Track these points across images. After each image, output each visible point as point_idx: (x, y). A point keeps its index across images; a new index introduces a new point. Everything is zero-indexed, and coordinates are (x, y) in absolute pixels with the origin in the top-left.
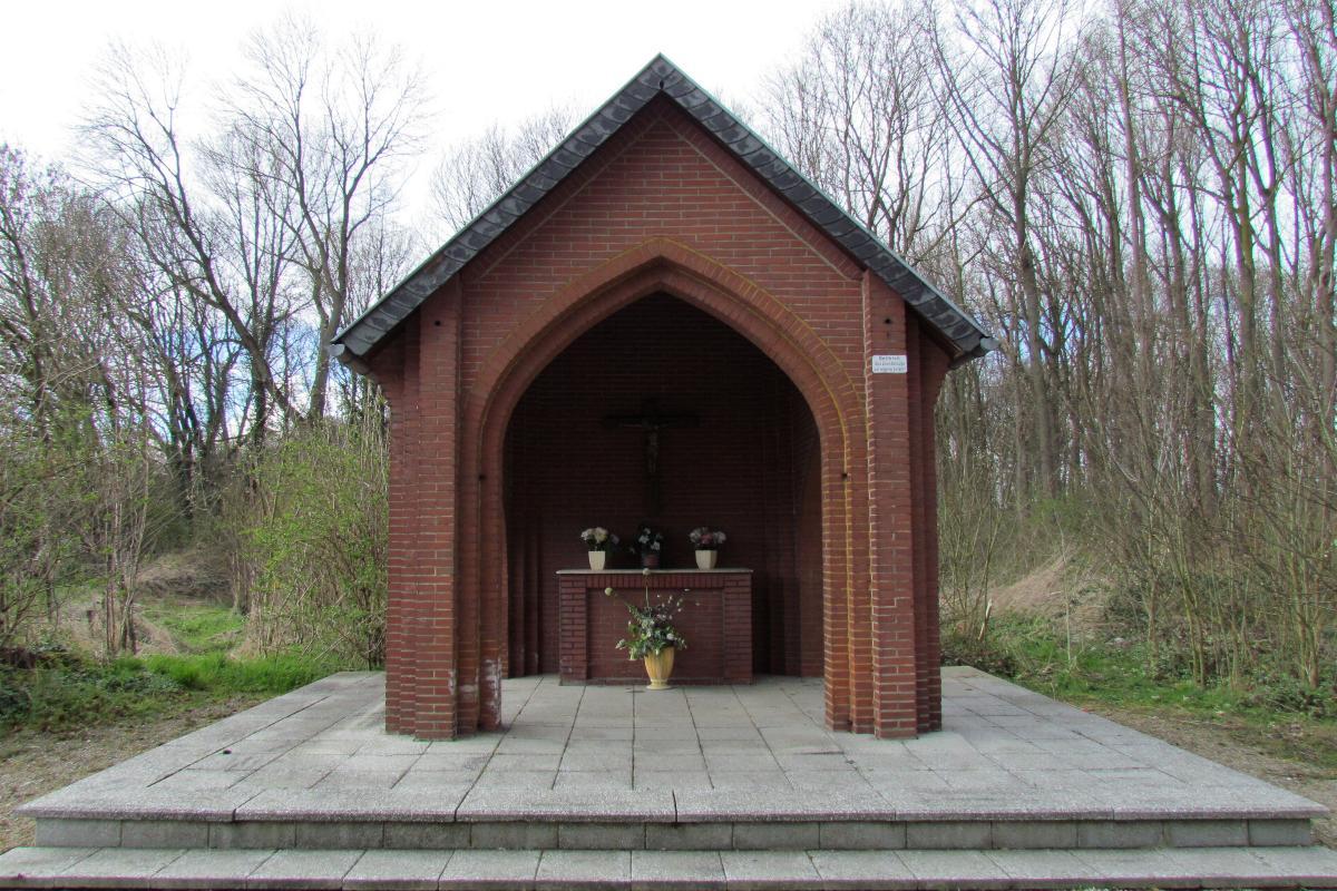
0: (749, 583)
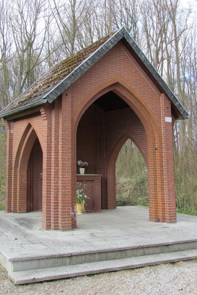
0: (100, 179)
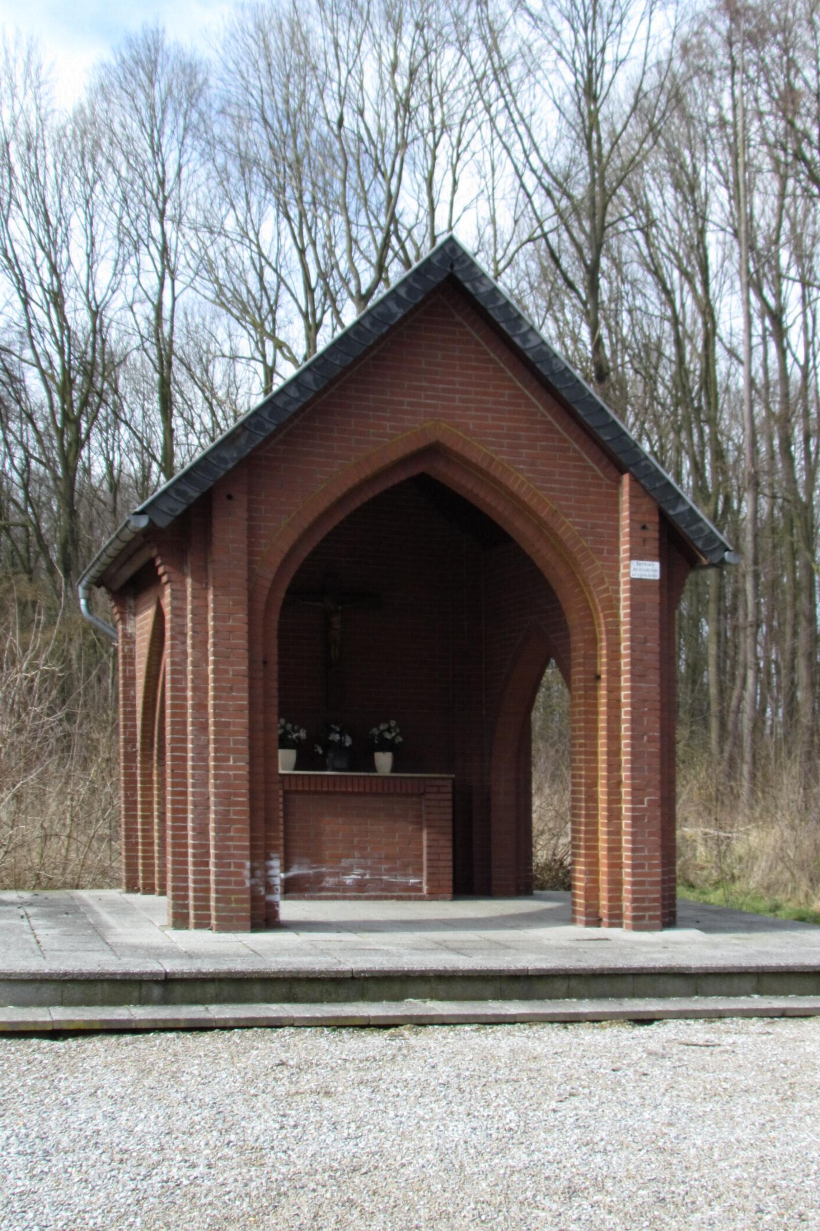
0: (450, 789)
